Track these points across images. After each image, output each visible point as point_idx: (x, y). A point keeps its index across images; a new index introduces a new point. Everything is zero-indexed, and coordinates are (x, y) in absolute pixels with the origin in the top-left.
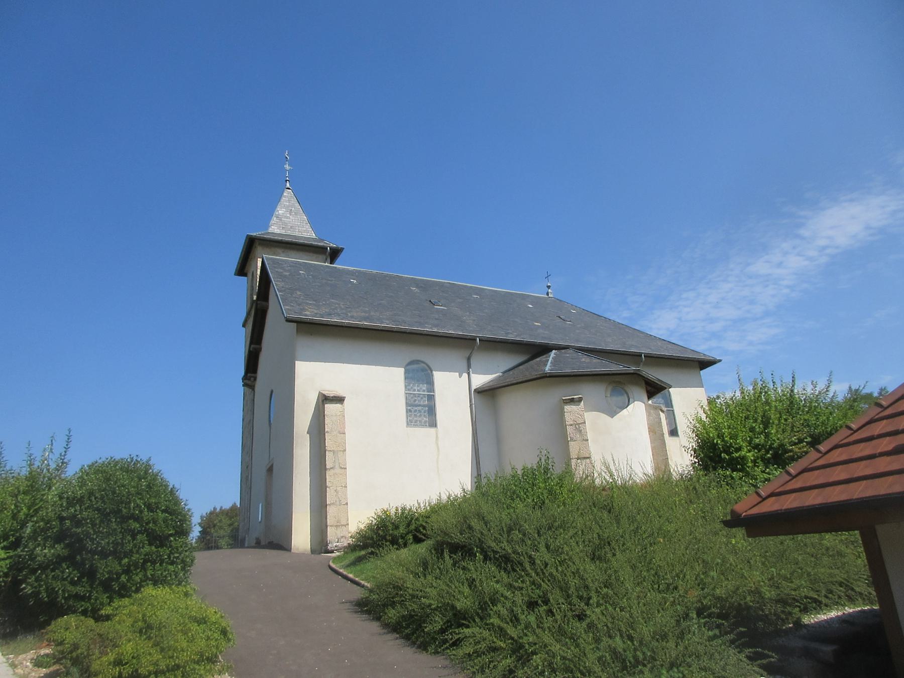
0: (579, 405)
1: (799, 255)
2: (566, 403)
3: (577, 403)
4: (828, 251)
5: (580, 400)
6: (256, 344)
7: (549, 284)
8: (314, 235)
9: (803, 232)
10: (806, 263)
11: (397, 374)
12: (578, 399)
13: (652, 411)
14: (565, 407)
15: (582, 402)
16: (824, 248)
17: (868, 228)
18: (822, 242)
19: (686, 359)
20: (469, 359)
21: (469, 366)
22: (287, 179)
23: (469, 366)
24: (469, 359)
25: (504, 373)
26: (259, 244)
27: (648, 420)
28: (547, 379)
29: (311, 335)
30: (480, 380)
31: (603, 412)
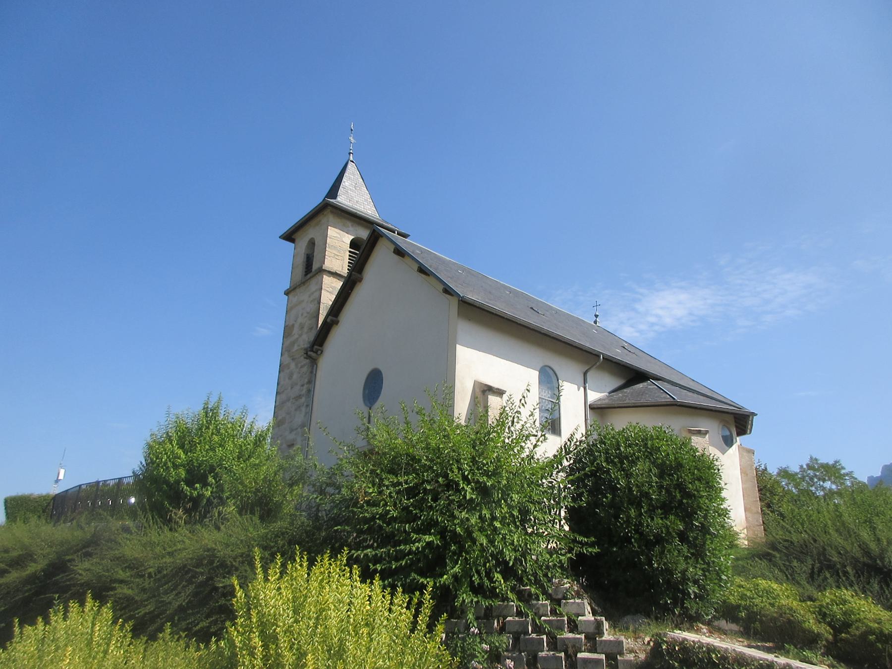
0: (704, 438)
1: (632, 326)
2: (694, 434)
3: (704, 436)
4: (656, 328)
5: (706, 432)
6: (333, 316)
7: (597, 314)
8: (377, 215)
9: (638, 306)
10: (637, 334)
11: (533, 376)
12: (704, 432)
13: (745, 454)
14: (692, 437)
15: (707, 436)
16: (653, 324)
17: (691, 314)
18: (652, 319)
19: (679, 404)
20: (585, 374)
21: (585, 382)
22: (351, 151)
23: (585, 382)
24: (585, 374)
25: (610, 393)
26: (332, 212)
27: (741, 461)
28: (675, 407)
29: (469, 320)
30: (594, 396)
31: (716, 447)
